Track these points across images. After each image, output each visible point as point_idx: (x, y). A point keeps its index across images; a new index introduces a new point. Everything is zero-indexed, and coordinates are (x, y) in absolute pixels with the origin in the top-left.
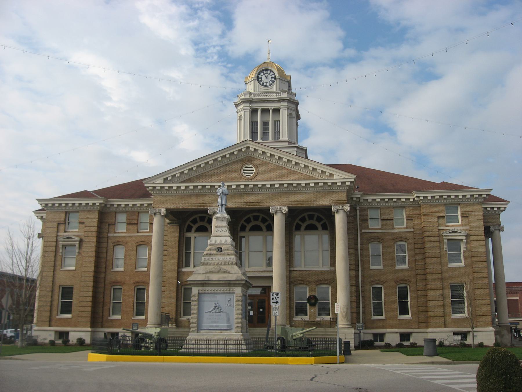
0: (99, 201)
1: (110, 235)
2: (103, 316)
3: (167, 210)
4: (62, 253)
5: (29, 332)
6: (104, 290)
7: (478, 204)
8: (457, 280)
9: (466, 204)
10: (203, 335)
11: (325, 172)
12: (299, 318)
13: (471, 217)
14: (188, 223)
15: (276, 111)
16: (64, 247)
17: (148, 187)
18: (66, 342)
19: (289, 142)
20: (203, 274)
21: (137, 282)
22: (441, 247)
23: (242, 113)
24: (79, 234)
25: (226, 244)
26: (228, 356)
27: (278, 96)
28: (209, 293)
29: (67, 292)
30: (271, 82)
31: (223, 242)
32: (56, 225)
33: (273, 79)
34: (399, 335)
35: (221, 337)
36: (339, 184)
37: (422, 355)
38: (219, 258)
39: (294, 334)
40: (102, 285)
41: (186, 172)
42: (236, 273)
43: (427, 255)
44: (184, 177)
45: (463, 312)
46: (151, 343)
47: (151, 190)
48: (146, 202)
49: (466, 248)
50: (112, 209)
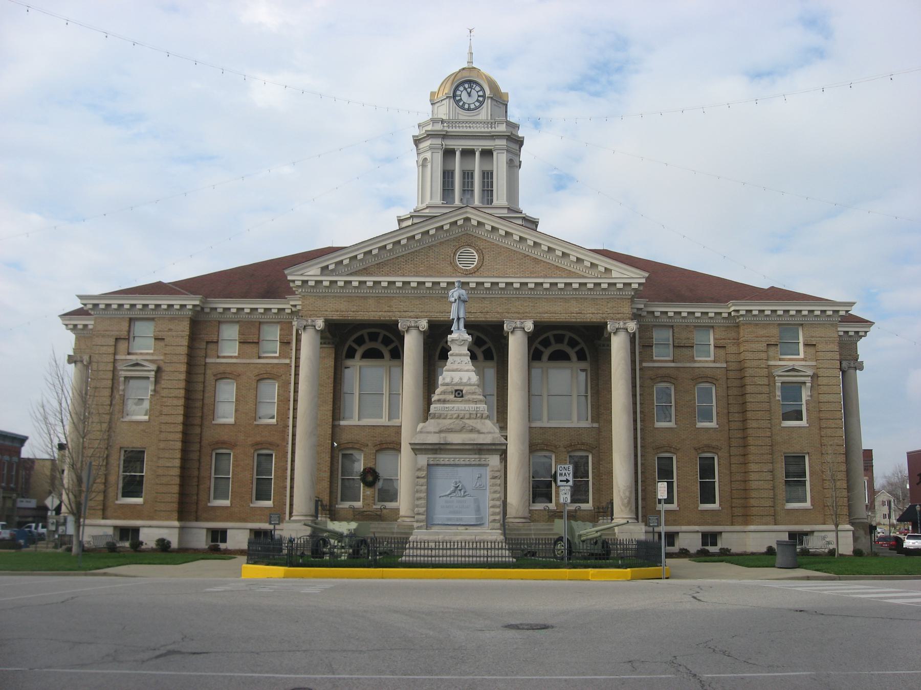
0: (191, 302)
1: (209, 360)
2: (198, 500)
3: (429, 322)
4: (124, 390)
5: (61, 529)
6: (200, 456)
7: (832, 325)
8: (795, 448)
9: (812, 325)
10: (438, 534)
11: (597, 265)
12: (346, 505)
13: (820, 347)
14: (350, 342)
15: (487, 154)
16: (127, 378)
17: (294, 281)
18: (136, 545)
19: (508, 208)
20: (435, 433)
21: (257, 444)
22: (771, 394)
23: (428, 155)
24: (155, 358)
25: (470, 385)
26: (422, 567)
27: (490, 130)
28: (444, 465)
29: (134, 458)
30: (477, 104)
31: (465, 380)
32: (112, 341)
33: (481, 99)
34: (700, 534)
35: (468, 538)
36: (620, 286)
37: (774, 566)
38: (460, 407)
39: (581, 532)
40: (196, 447)
41: (360, 257)
42: (490, 433)
43: (749, 406)
44: (357, 266)
45: (805, 501)
46: (342, 547)
47: (298, 286)
48: (274, 305)
49: (811, 396)
50: (214, 316)
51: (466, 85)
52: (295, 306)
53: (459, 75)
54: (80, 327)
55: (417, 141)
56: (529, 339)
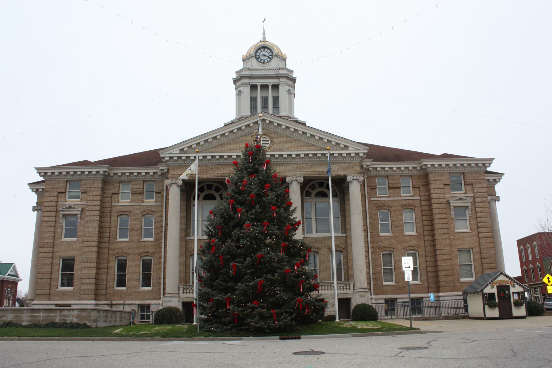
0: (102, 169)
3: (304, 177)
8: (68, 254)
15: (276, 87)
17: (164, 158)
33: (271, 57)
51: (264, 51)
52: (163, 170)
53: (258, 45)
54: (41, 190)
55: (235, 81)
56: (301, 187)
